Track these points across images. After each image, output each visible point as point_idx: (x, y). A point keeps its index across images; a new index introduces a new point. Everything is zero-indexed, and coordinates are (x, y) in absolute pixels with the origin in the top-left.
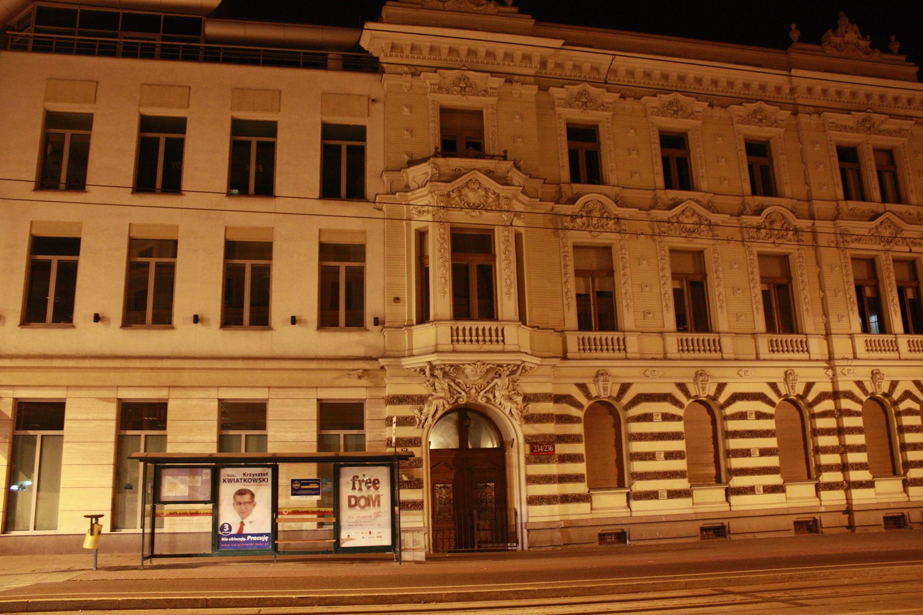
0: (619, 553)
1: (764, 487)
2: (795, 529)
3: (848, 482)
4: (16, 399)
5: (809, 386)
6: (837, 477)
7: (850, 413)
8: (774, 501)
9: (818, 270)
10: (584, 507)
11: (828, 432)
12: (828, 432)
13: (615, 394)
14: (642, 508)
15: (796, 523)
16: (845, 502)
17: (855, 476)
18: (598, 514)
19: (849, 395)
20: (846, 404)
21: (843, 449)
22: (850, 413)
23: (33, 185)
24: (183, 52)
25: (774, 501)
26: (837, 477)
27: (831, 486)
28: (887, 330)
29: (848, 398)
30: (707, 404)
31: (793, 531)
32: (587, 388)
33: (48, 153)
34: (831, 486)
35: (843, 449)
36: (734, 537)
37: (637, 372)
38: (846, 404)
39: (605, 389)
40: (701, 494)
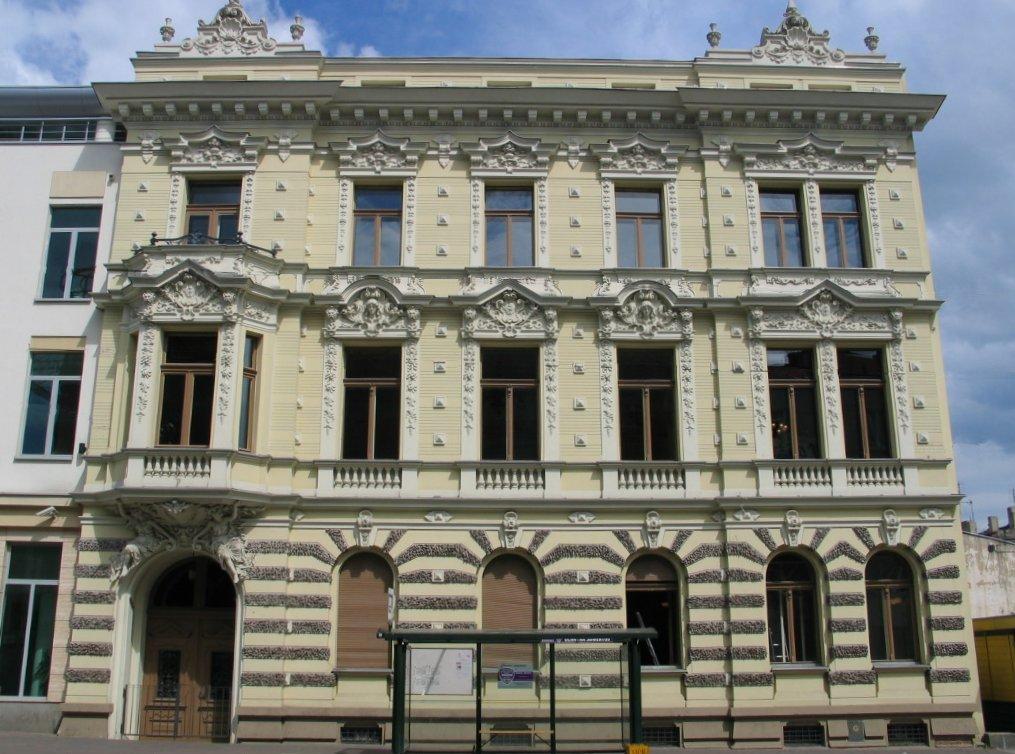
0: (350, 742)
2: (785, 739)
3: (733, 677)
6: (716, 667)
7: (742, 576)
9: (713, 367)
11: (708, 603)
12: (708, 603)
17: (741, 667)
20: (736, 562)
21: (730, 629)
22: (742, 576)
24: (84, 134)
26: (716, 667)
27: (703, 681)
28: (107, 711)
31: (782, 740)
33: (35, 671)
34: (703, 681)
35: (730, 629)
36: (833, 743)
38: (736, 562)
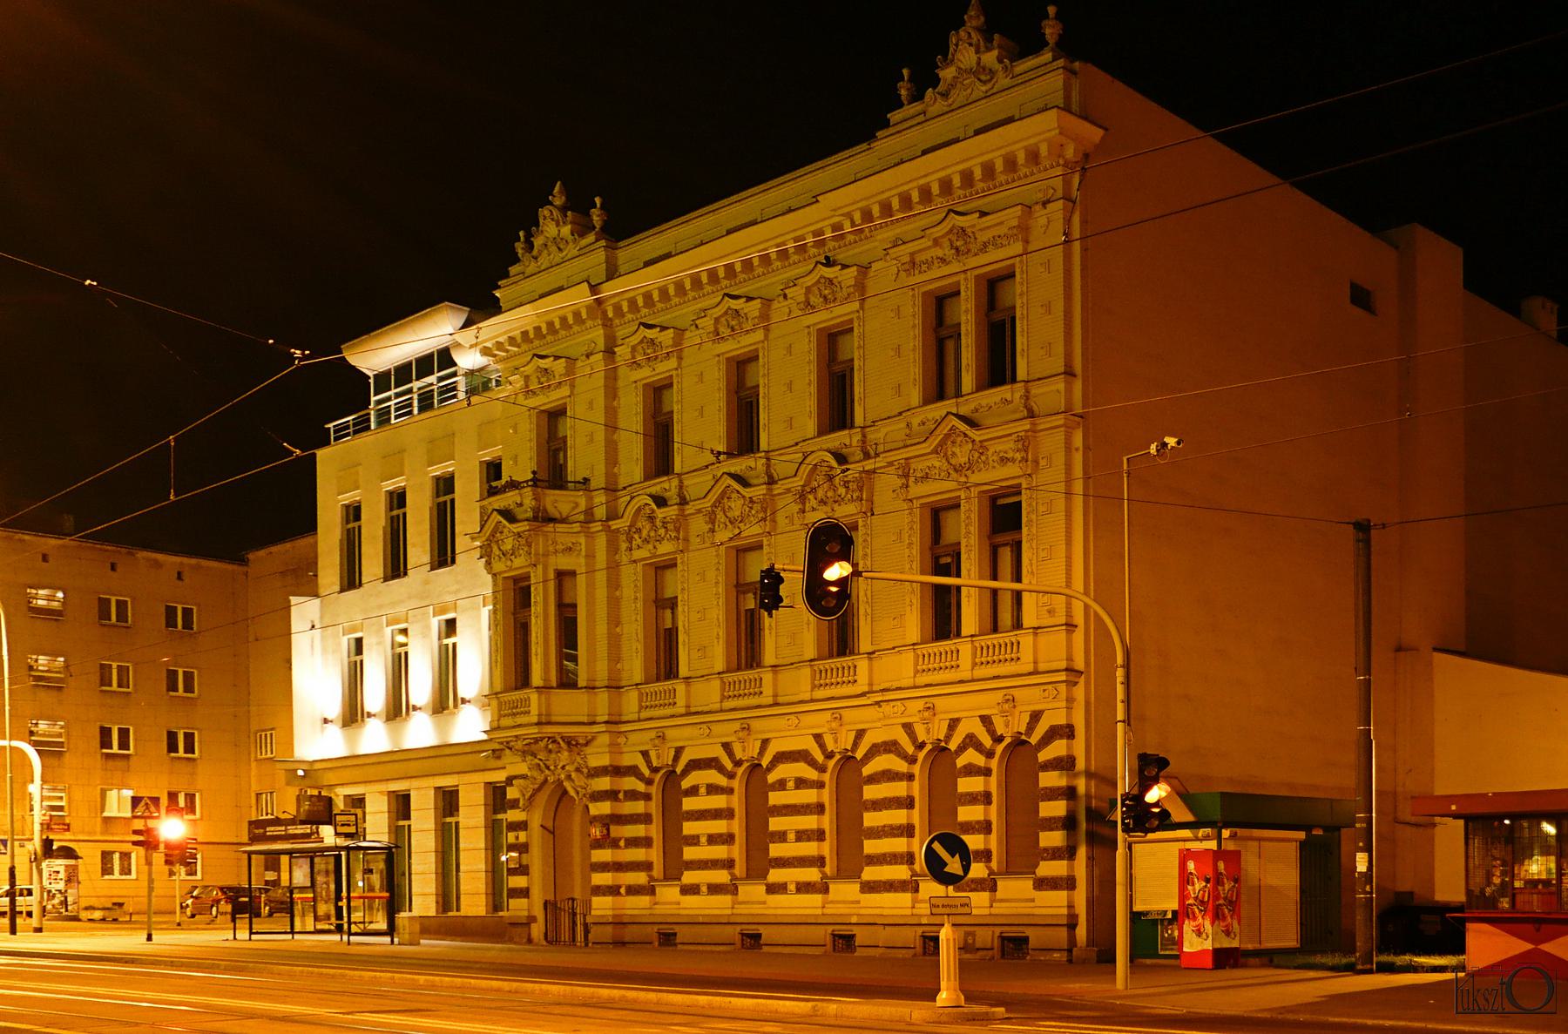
1: (798, 884)
4: (437, 789)
5: (1036, 717)
8: (810, 904)
10: (643, 901)
13: (1023, 729)
14: (691, 901)
15: (1002, 938)
16: (1065, 911)
18: (659, 910)
19: (633, 771)
23: (428, 567)
25: (810, 904)
29: (890, 752)
30: (755, 769)
32: (991, 723)
36: (765, 949)
37: (694, 731)
39: (928, 732)
40: (1007, 887)
